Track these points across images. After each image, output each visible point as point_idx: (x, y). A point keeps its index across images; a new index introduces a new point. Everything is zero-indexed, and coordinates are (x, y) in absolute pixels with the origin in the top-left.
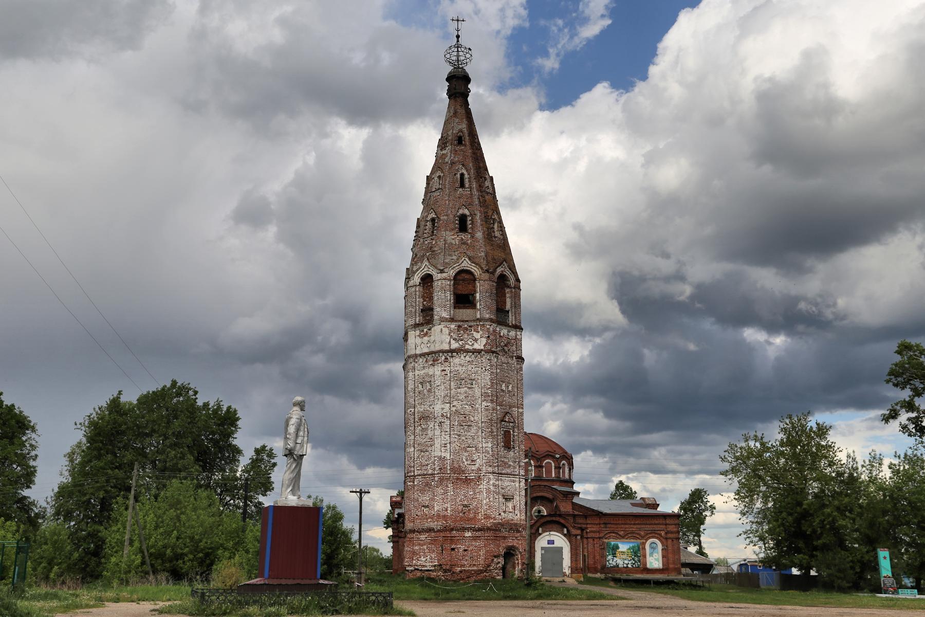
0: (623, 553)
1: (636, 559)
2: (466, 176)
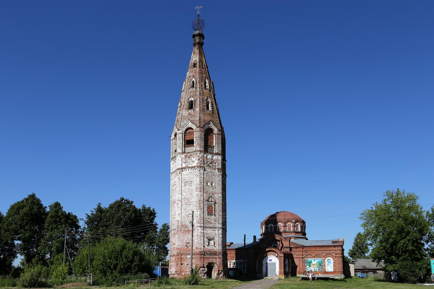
0: (314, 264)
1: (320, 267)
2: (195, 82)
